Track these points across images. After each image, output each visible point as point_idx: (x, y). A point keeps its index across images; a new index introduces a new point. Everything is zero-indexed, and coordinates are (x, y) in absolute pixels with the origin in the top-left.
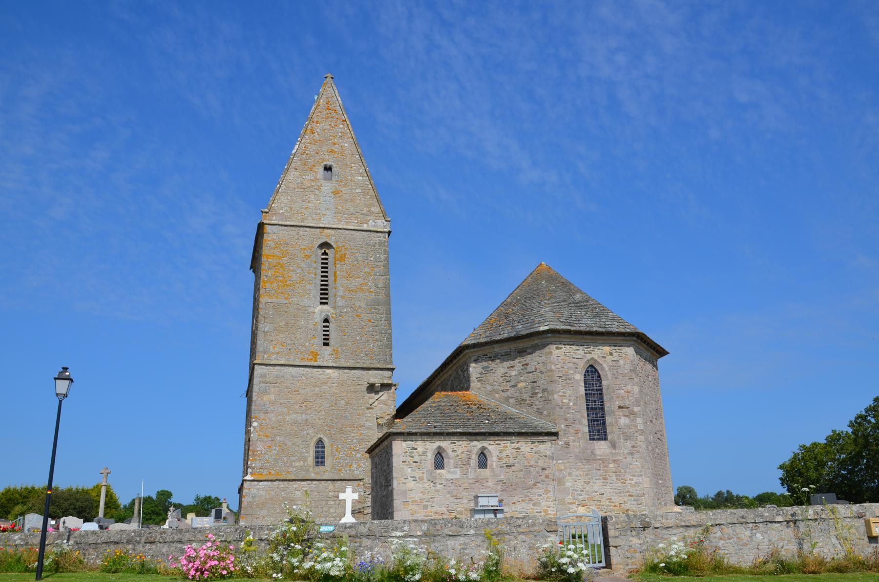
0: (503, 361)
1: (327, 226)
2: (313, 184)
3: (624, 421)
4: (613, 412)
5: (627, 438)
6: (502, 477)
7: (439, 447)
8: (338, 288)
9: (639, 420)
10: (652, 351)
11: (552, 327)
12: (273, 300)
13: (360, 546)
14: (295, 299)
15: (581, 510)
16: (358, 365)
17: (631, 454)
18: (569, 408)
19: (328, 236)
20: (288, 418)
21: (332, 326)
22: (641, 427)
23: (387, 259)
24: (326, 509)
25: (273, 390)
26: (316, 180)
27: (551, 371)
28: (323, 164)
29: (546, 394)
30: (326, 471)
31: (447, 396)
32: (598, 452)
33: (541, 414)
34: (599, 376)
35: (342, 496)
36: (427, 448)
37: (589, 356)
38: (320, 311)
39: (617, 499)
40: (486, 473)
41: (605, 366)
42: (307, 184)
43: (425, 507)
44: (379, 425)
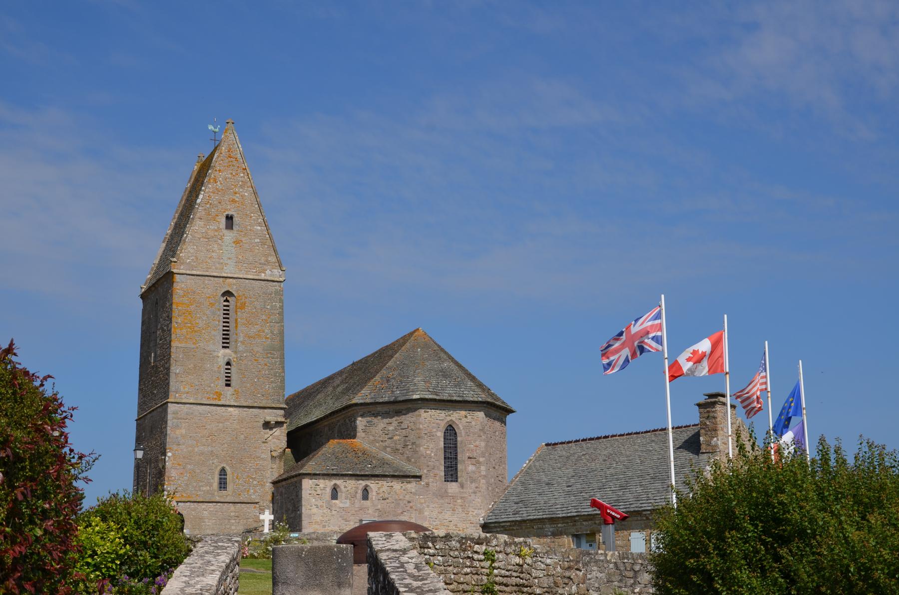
0: (383, 418)
1: (229, 275)
3: (471, 468)
4: (464, 461)
5: (473, 481)
7: (335, 484)
8: (240, 334)
9: (483, 468)
10: (498, 411)
11: (422, 396)
12: (183, 345)
14: (201, 344)
16: (255, 405)
17: (475, 493)
19: (230, 285)
21: (234, 369)
22: (483, 473)
23: (282, 307)
25: (184, 425)
26: (219, 229)
27: (419, 429)
28: (225, 214)
30: (229, 494)
31: (339, 443)
32: (450, 491)
33: (410, 461)
35: (262, 517)
36: (326, 485)
37: (449, 418)
38: (223, 354)
39: (461, 526)
40: (367, 503)
41: (460, 426)
42: (211, 233)
44: (272, 457)
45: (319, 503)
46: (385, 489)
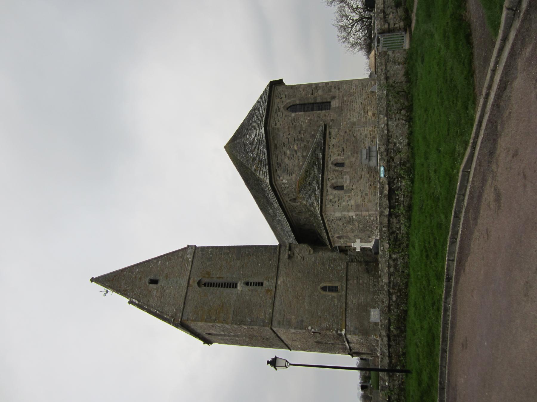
2: (159, 290)
6: (349, 153)
8: (227, 277)
13: (393, 149)
15: (370, 114)
17: (339, 89)
18: (311, 120)
19: (194, 281)
20: (307, 308)
21: (251, 280)
24: (365, 285)
25: (288, 317)
29: (302, 132)
32: (337, 105)
34: (294, 105)
35: (358, 250)
39: (364, 96)
40: (347, 162)
41: (288, 101)
42: (159, 294)
43: (366, 194)
45: (346, 198)
46: (335, 150)
